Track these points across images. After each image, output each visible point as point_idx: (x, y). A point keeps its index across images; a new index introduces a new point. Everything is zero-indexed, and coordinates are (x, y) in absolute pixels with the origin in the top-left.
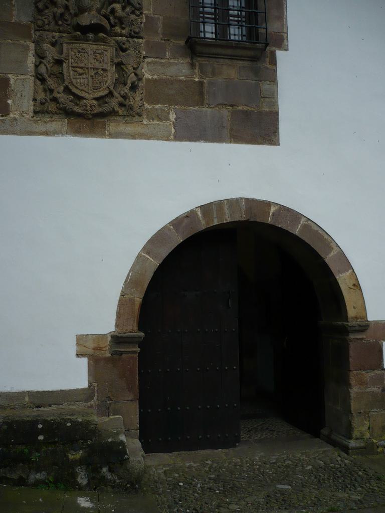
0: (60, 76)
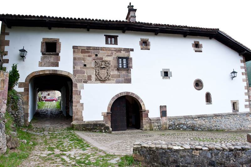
0: (99, 75)
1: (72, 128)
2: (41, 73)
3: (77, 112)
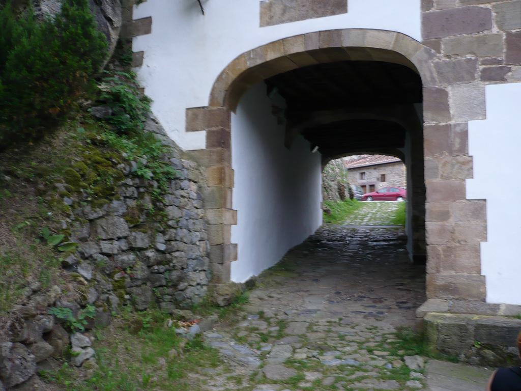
1: (418, 339)
2: (271, 56)
3: (449, 250)
